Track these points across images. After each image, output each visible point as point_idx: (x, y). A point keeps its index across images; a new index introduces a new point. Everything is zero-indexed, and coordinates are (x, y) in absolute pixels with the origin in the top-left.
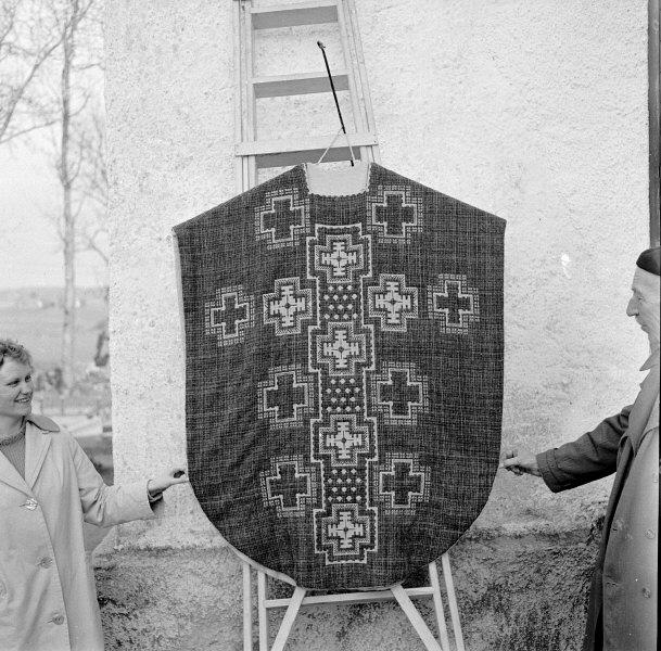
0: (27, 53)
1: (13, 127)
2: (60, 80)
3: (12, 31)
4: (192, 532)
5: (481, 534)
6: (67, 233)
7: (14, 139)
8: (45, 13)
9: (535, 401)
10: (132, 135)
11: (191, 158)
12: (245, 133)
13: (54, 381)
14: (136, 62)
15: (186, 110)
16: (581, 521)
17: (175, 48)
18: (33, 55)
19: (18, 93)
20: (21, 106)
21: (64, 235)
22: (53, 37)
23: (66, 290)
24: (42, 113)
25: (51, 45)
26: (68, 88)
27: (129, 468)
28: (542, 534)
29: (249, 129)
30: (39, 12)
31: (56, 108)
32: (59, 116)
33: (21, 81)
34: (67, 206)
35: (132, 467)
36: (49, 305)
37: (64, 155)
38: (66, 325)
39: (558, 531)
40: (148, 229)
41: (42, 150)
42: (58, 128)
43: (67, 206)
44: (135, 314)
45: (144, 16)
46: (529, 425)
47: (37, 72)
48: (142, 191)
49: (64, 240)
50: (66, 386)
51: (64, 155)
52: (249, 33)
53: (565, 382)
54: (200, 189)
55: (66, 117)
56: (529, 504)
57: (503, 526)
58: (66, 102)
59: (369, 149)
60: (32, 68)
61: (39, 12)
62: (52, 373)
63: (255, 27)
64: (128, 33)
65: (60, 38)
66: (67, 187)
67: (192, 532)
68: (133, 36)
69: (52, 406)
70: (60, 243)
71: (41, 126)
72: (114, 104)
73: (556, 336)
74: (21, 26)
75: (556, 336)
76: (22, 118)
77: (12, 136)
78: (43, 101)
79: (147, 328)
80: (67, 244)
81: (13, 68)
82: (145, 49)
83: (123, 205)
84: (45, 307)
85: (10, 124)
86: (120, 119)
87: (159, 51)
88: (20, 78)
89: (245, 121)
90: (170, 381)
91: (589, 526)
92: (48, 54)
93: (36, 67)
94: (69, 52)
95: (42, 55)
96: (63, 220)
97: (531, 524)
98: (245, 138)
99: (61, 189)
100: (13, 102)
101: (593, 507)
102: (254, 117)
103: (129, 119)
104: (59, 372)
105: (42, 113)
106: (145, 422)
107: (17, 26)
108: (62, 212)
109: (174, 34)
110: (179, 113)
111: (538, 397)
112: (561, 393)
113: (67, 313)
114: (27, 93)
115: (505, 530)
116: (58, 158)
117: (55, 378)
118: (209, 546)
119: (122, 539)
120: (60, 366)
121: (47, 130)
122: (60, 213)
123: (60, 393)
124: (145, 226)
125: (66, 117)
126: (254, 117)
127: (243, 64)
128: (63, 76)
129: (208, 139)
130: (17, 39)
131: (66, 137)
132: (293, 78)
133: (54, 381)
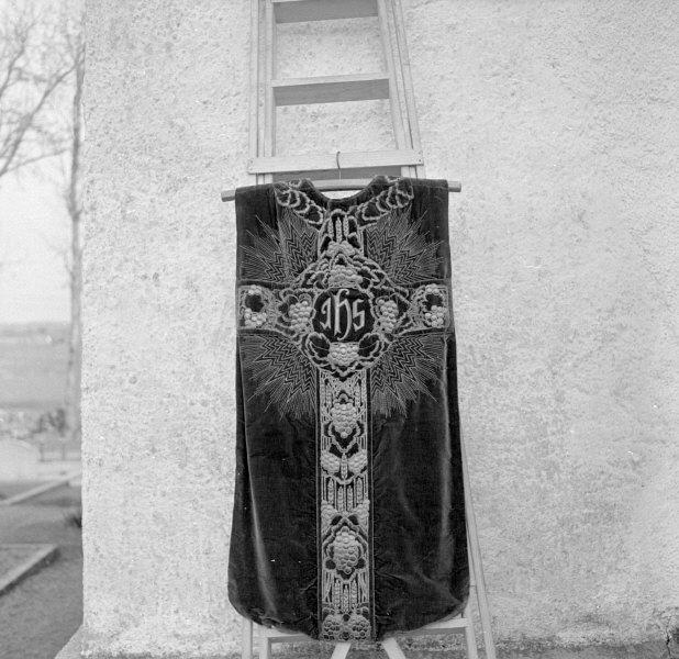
0: (38, 80)
1: (20, 156)
2: (71, 107)
3: (22, 57)
4: (177, 636)
5: (530, 644)
6: (74, 268)
7: (22, 168)
8: (59, 38)
9: (599, 482)
10: (115, 151)
11: (185, 180)
12: (261, 146)
13: (56, 423)
14: (121, 63)
15: (180, 121)
16: (654, 631)
17: (169, 47)
18: (44, 81)
19: (27, 122)
20: (30, 134)
21: (71, 268)
22: (65, 64)
23: (72, 326)
24: (52, 141)
25: (63, 71)
26: (79, 115)
27: (101, 556)
28: (605, 647)
29: (266, 143)
30: (52, 37)
31: (66, 136)
32: (69, 144)
33: (30, 108)
34: (75, 239)
35: (105, 554)
36: (57, 341)
37: (73, 185)
38: (70, 363)
39: (626, 642)
40: (130, 265)
41: (50, 179)
42: (67, 158)
43: (75, 239)
44: (113, 367)
45: (132, 9)
46: (592, 511)
47: (48, 98)
48: (124, 218)
49: (71, 273)
50: (68, 428)
51: (73, 185)
52: (270, 26)
53: (636, 459)
54: (195, 218)
55: (77, 145)
56: (589, 608)
57: (560, 635)
58: (77, 130)
59: (413, 169)
60: (41, 95)
61: (52, 37)
62: (55, 414)
63: (278, 21)
64: (113, 28)
65: (72, 63)
66: (76, 218)
67: (177, 636)
68: (118, 33)
69: (53, 450)
70: (66, 278)
71: (48, 155)
72: (94, 114)
73: (625, 402)
74: (32, 51)
75: (625, 402)
76: (31, 145)
77: (18, 165)
78: (53, 130)
79: (127, 385)
80: (74, 278)
81: (22, 95)
82: (132, 47)
83: (101, 235)
84: (55, 342)
85: (18, 152)
86: (101, 132)
87: (148, 49)
88: (30, 104)
89: (262, 132)
90: (154, 451)
91: (664, 637)
92: (60, 80)
93: (47, 94)
94: (80, 75)
95: (54, 80)
96: (70, 254)
97: (592, 633)
98: (261, 151)
99: (69, 221)
100: (21, 130)
101: (668, 614)
102: (274, 126)
103: (111, 131)
104: (62, 413)
105: (52, 141)
106: (122, 501)
107: (28, 50)
108: (70, 245)
109: (167, 31)
110: (172, 125)
111: (603, 477)
112: (630, 473)
113: (72, 351)
114: (37, 120)
115: (559, 639)
116: (67, 187)
117: (58, 419)
118: (196, 653)
119: (91, 643)
120: (63, 406)
121: (56, 159)
122: (67, 245)
123: (63, 436)
124: (127, 261)
125: (77, 145)
126: (274, 126)
127: (262, 67)
128: (74, 103)
129: (205, 157)
130: (27, 64)
131: (75, 166)
132: (322, 82)
133: (56, 423)
